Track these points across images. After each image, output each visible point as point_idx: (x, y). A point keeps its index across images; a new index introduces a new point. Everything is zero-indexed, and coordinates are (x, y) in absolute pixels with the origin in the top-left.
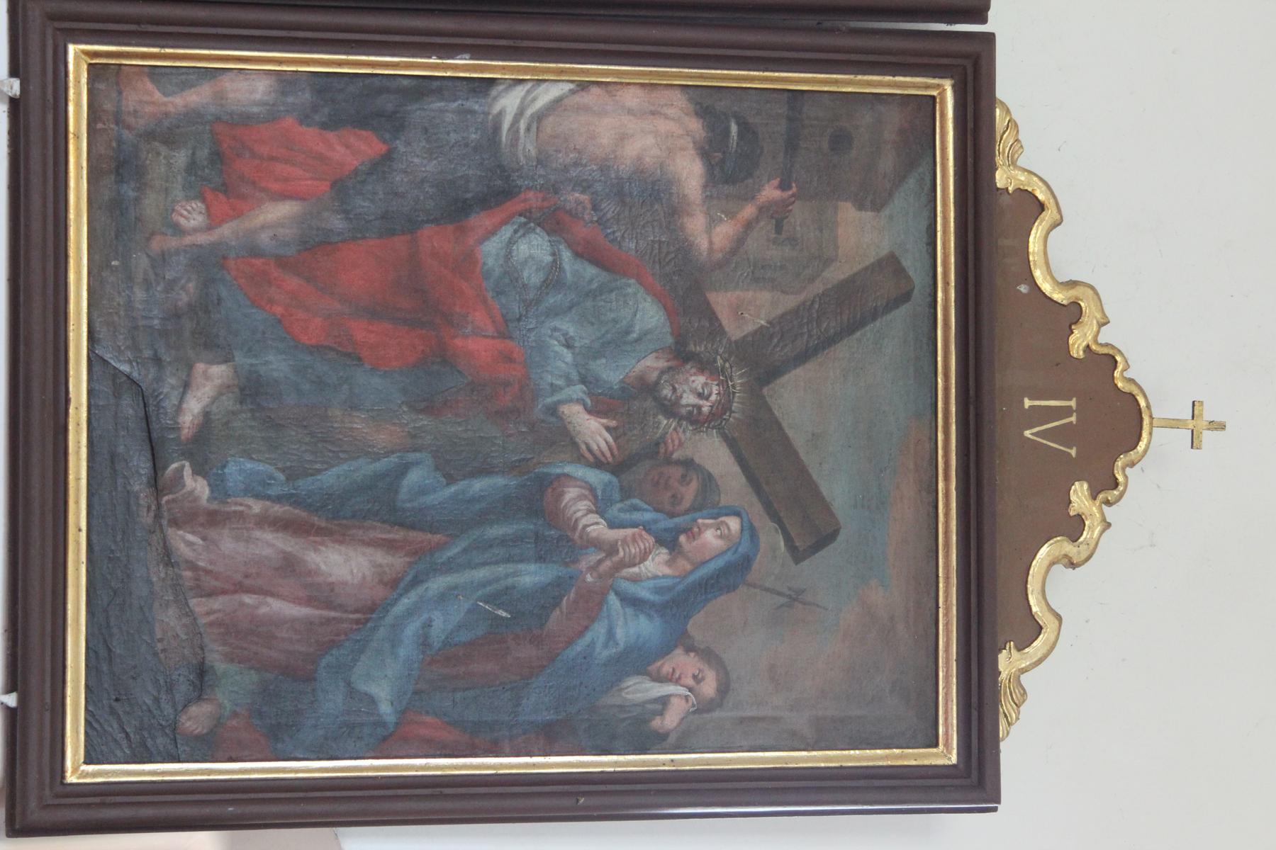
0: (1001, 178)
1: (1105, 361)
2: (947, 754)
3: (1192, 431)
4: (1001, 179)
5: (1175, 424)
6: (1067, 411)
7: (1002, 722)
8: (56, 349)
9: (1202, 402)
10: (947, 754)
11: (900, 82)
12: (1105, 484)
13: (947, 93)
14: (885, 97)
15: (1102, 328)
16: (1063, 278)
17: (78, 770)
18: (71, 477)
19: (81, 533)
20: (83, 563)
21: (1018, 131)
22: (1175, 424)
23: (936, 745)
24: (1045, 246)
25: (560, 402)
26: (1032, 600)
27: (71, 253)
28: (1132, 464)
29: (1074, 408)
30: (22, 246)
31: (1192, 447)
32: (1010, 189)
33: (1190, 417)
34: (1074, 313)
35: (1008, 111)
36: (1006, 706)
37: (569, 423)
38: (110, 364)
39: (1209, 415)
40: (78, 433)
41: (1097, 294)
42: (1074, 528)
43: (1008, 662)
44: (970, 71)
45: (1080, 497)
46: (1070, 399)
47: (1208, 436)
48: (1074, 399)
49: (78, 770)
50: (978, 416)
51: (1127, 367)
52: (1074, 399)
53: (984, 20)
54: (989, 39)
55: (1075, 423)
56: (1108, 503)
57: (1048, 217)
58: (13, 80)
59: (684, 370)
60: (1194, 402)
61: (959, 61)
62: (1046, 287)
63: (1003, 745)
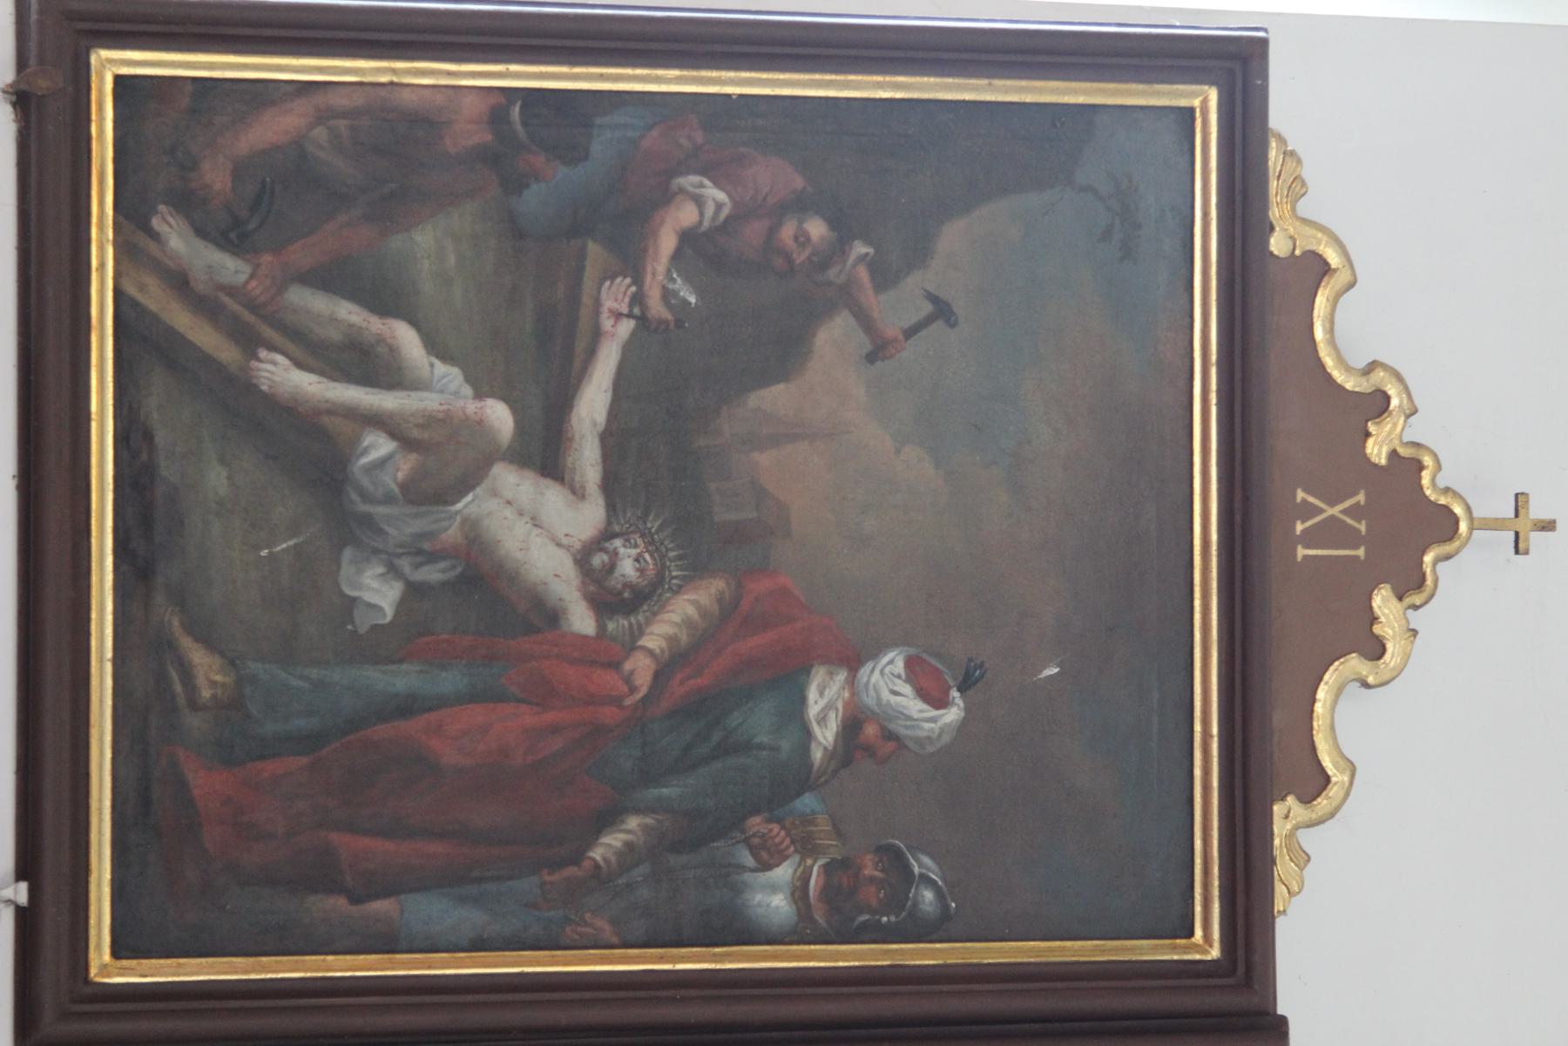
1: (1406, 467)
2: (1207, 100)
3: (1517, 534)
4: (1278, 245)
5: (1495, 524)
7: (1280, 890)
11: (902, 82)
12: (1411, 584)
14: (282, 84)
16: (1361, 363)
22: (1495, 524)
24: (1335, 739)
25: (397, 483)
28: (1448, 557)
31: (1517, 552)
34: (1378, 404)
36: (1284, 867)
37: (576, 449)
39: (1537, 511)
43: (1286, 815)
45: (1383, 601)
47: (1536, 539)
48: (1299, 558)
50: (1246, 499)
51: (1439, 467)
55: (1362, 503)
57: (1342, 278)
59: (219, 691)
63: (1281, 925)
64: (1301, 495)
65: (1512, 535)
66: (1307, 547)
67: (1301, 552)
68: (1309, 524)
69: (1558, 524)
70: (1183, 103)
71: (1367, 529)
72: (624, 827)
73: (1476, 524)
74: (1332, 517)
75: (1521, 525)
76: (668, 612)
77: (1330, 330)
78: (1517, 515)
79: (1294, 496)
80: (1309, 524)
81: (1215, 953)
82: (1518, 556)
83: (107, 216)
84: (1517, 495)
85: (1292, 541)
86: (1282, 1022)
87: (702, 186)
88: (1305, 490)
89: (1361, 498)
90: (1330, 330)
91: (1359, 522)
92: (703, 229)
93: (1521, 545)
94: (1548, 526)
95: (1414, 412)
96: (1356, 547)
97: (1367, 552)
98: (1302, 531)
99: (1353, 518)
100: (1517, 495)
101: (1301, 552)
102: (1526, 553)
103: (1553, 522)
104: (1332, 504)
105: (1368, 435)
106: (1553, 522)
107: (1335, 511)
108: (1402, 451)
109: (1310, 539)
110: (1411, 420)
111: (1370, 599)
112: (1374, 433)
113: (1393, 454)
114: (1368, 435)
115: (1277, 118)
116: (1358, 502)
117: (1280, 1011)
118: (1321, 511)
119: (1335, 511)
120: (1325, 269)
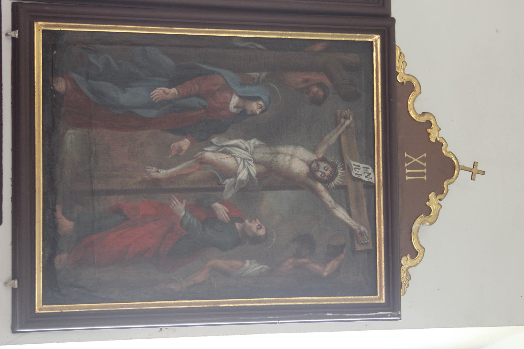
1: (439, 145)
9: (478, 163)
10: (376, 39)
12: (440, 191)
13: (376, 39)
15: (439, 132)
17: (39, 307)
19: (40, 31)
21: (404, 55)
27: (35, 84)
28: (452, 183)
31: (471, 179)
33: (472, 167)
35: (400, 49)
38: (219, 180)
39: (480, 167)
41: (435, 118)
42: (428, 211)
43: (406, 261)
46: (409, 179)
48: (407, 179)
49: (39, 27)
52: (407, 179)
56: (440, 200)
60: (474, 162)
62: (413, 116)
66: (408, 169)
68: (408, 164)
69: (486, 173)
70: (370, 40)
71: (427, 179)
73: (460, 168)
75: (474, 170)
76: (239, 173)
78: (473, 168)
80: (408, 164)
81: (383, 301)
82: (476, 179)
83: (40, 53)
85: (405, 174)
86: (393, 20)
87: (158, 175)
89: (425, 155)
91: (424, 163)
94: (473, 179)
96: (424, 176)
97: (427, 171)
98: (407, 166)
99: (422, 162)
101: (407, 178)
102: (474, 180)
103: (484, 172)
105: (429, 134)
106: (484, 172)
108: (438, 139)
109: (409, 168)
113: (436, 140)
114: (429, 134)
117: (392, 16)
118: (413, 160)
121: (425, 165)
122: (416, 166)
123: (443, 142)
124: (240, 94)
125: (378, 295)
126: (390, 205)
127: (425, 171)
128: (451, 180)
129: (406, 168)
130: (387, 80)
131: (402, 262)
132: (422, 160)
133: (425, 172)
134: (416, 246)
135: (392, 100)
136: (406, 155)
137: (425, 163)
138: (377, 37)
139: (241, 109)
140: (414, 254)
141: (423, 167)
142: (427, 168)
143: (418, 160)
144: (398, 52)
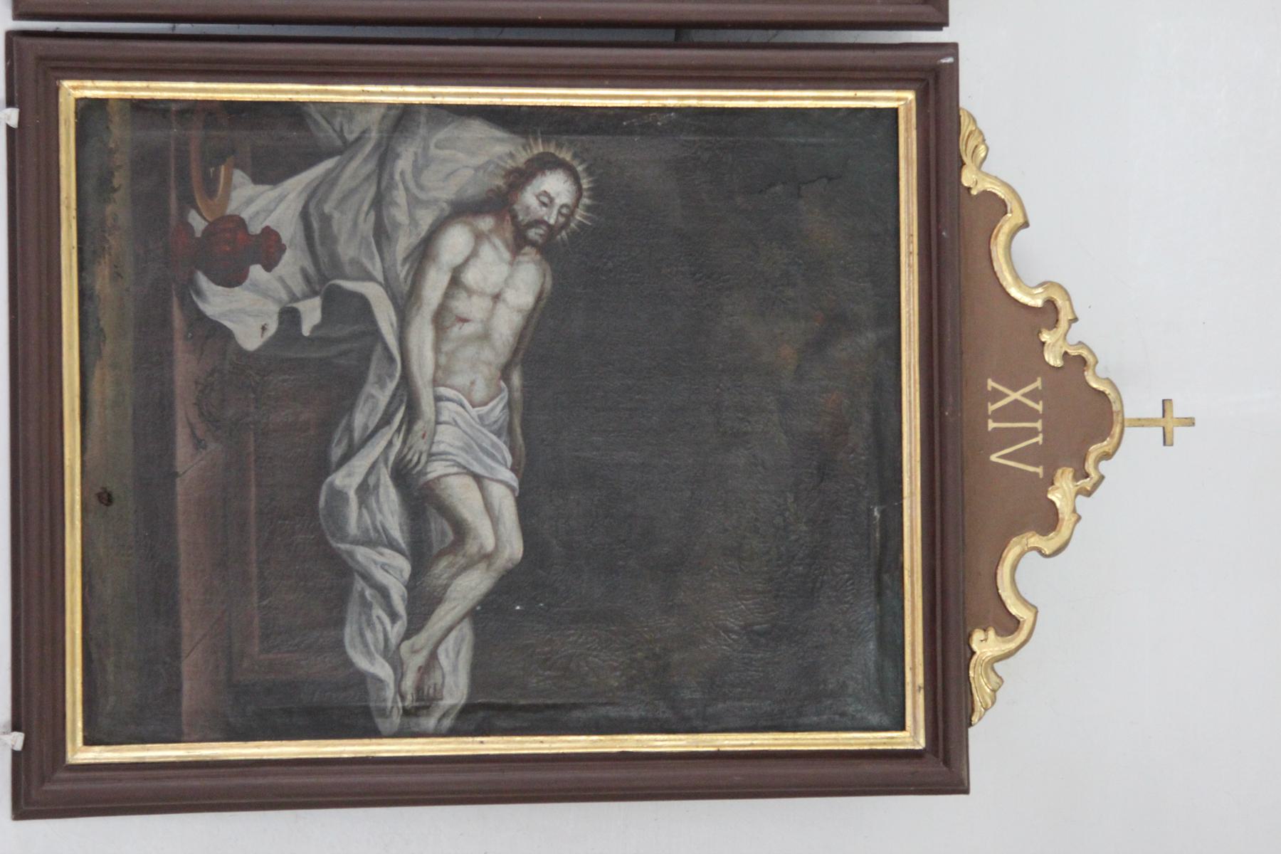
0: (968, 177)
1: (1076, 364)
2: (912, 737)
3: (1164, 428)
6: (1033, 433)
8: (52, 526)
9: (1171, 400)
10: (912, 737)
18: (67, 463)
20: (73, 248)
23: (902, 727)
26: (1014, 292)
29: (1040, 429)
30: (22, 645)
31: (1165, 443)
32: (974, 192)
33: (1160, 414)
39: (1178, 411)
40: (73, 667)
41: (1067, 293)
42: (1048, 520)
43: (985, 644)
44: (931, 82)
46: (995, 429)
48: (990, 429)
52: (990, 429)
53: (940, 23)
54: (952, 48)
55: (1040, 388)
58: (16, 734)
61: (922, 76)
64: (991, 384)
65: (1161, 429)
66: (995, 421)
67: (992, 425)
69: (1197, 422)
72: (435, 551)
74: (1015, 390)
77: (1014, 568)
78: (1164, 416)
79: (986, 385)
82: (1166, 447)
84: (1164, 401)
88: (994, 380)
89: (1038, 384)
90: (1014, 568)
91: (1037, 403)
92: (515, 484)
93: (1168, 441)
94: (1190, 422)
95: (1075, 320)
96: (1036, 421)
100: (1164, 401)
102: (1172, 445)
104: (1016, 402)
107: (1015, 396)
108: (1072, 352)
110: (1074, 325)
111: (1047, 364)
112: (1049, 341)
115: (964, 102)
116: (1037, 443)
119: (1015, 396)
120: (1002, 208)
121: (1039, 407)
122: (1016, 411)
123: (1085, 353)
124: (312, 209)
125: (882, 99)
126: (939, 632)
127: (1039, 425)
128: (1105, 445)
129: (989, 417)
130: (935, 321)
131: (975, 646)
132: (1032, 395)
133: (1041, 412)
134: (1015, 609)
135: (953, 769)
136: (991, 384)
137: (1041, 403)
138: (910, 95)
139: (388, 713)
140: (1009, 625)
141: (1033, 415)
142: (1043, 417)
143: (1025, 395)
144: (966, 127)
